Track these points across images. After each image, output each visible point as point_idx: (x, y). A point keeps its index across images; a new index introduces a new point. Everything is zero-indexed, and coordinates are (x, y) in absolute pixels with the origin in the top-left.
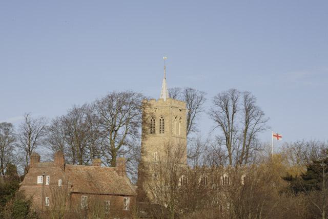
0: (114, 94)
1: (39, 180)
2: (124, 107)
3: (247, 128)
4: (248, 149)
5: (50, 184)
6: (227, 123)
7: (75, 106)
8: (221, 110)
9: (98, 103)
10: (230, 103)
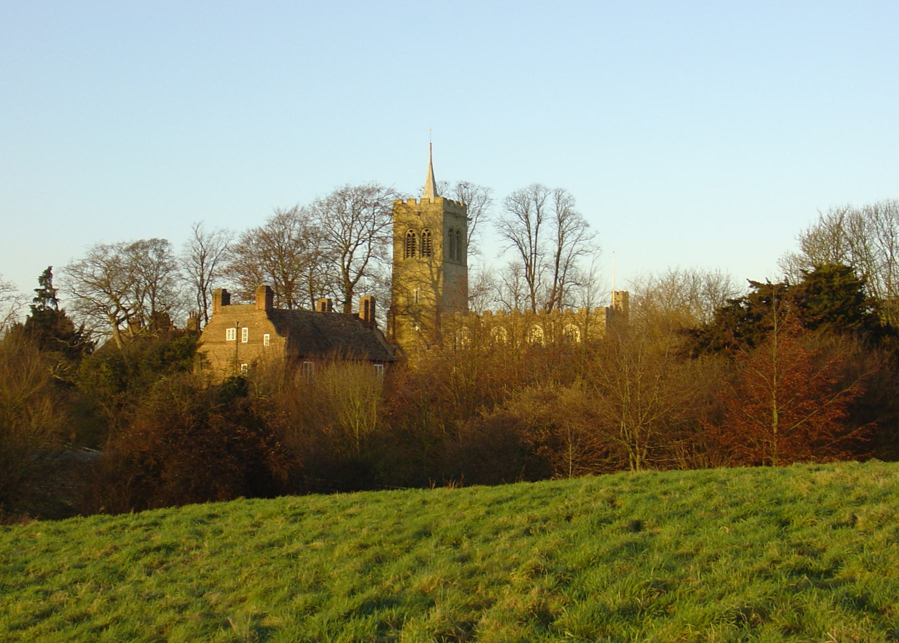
0: (347, 189)
1: (230, 334)
2: (364, 212)
3: (560, 249)
4: (561, 285)
5: (250, 342)
6: (526, 240)
7: (278, 210)
8: (517, 218)
9: (321, 205)
10: (533, 208)
